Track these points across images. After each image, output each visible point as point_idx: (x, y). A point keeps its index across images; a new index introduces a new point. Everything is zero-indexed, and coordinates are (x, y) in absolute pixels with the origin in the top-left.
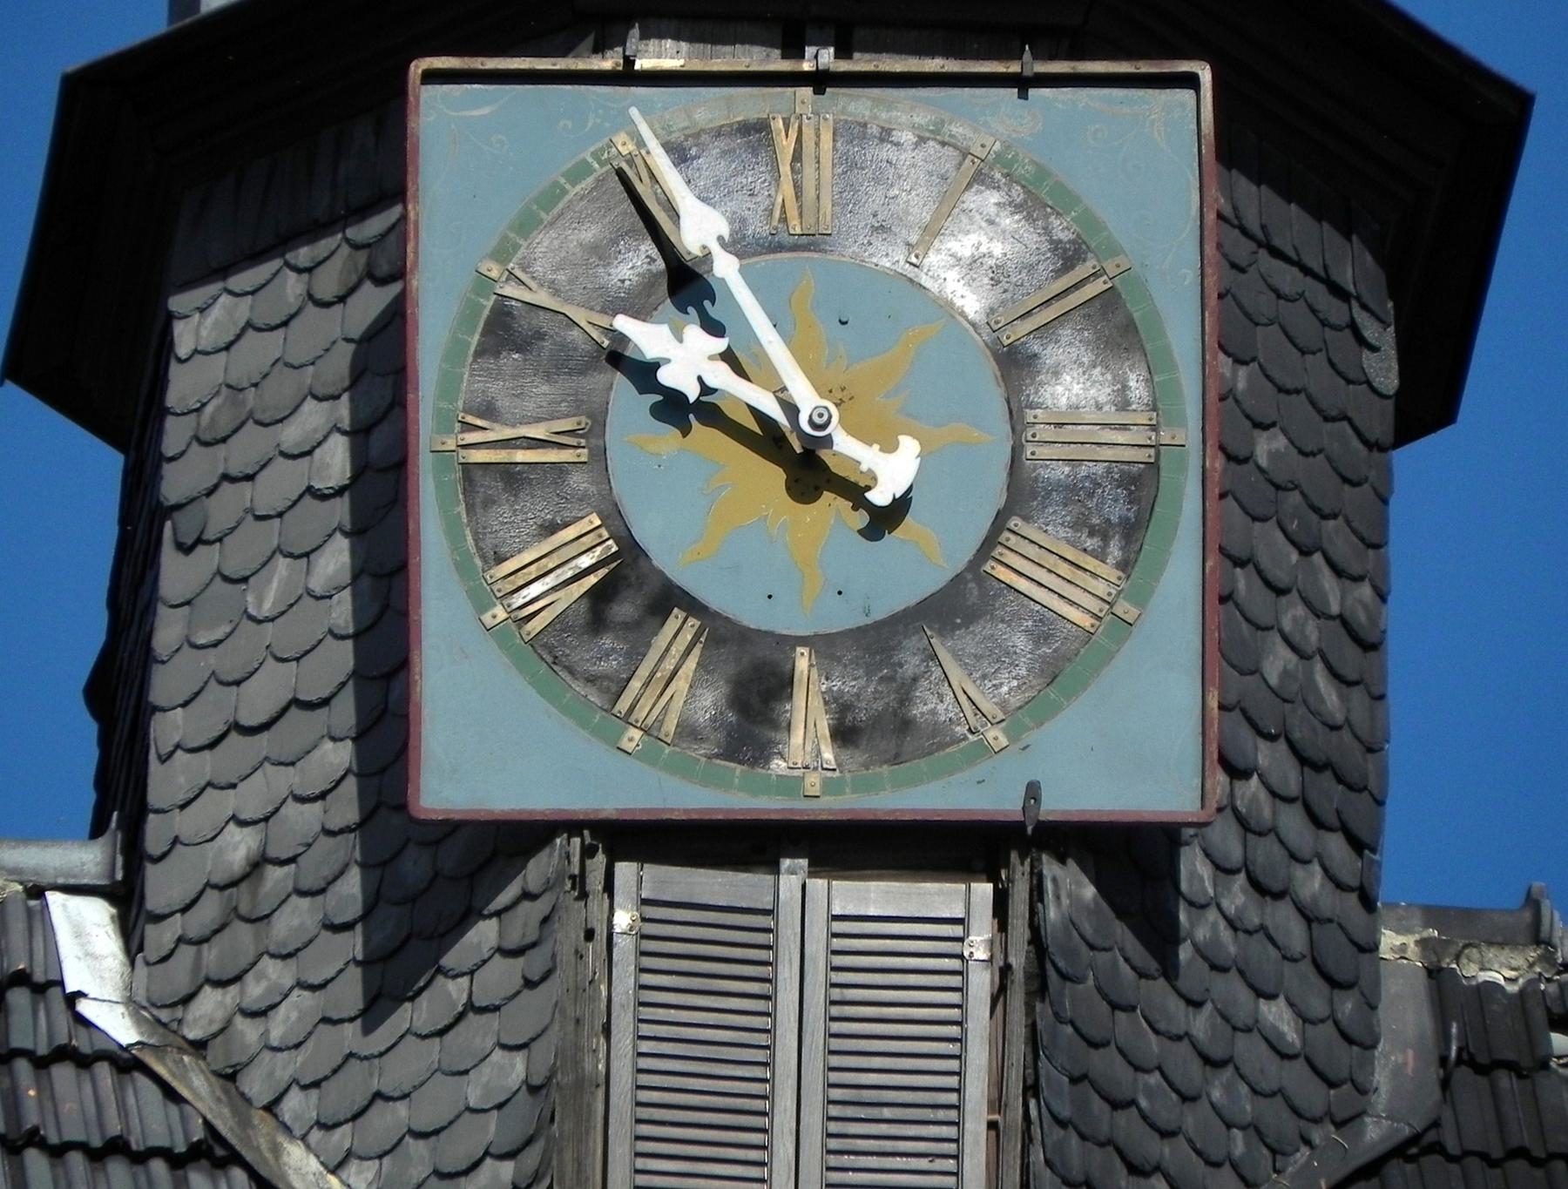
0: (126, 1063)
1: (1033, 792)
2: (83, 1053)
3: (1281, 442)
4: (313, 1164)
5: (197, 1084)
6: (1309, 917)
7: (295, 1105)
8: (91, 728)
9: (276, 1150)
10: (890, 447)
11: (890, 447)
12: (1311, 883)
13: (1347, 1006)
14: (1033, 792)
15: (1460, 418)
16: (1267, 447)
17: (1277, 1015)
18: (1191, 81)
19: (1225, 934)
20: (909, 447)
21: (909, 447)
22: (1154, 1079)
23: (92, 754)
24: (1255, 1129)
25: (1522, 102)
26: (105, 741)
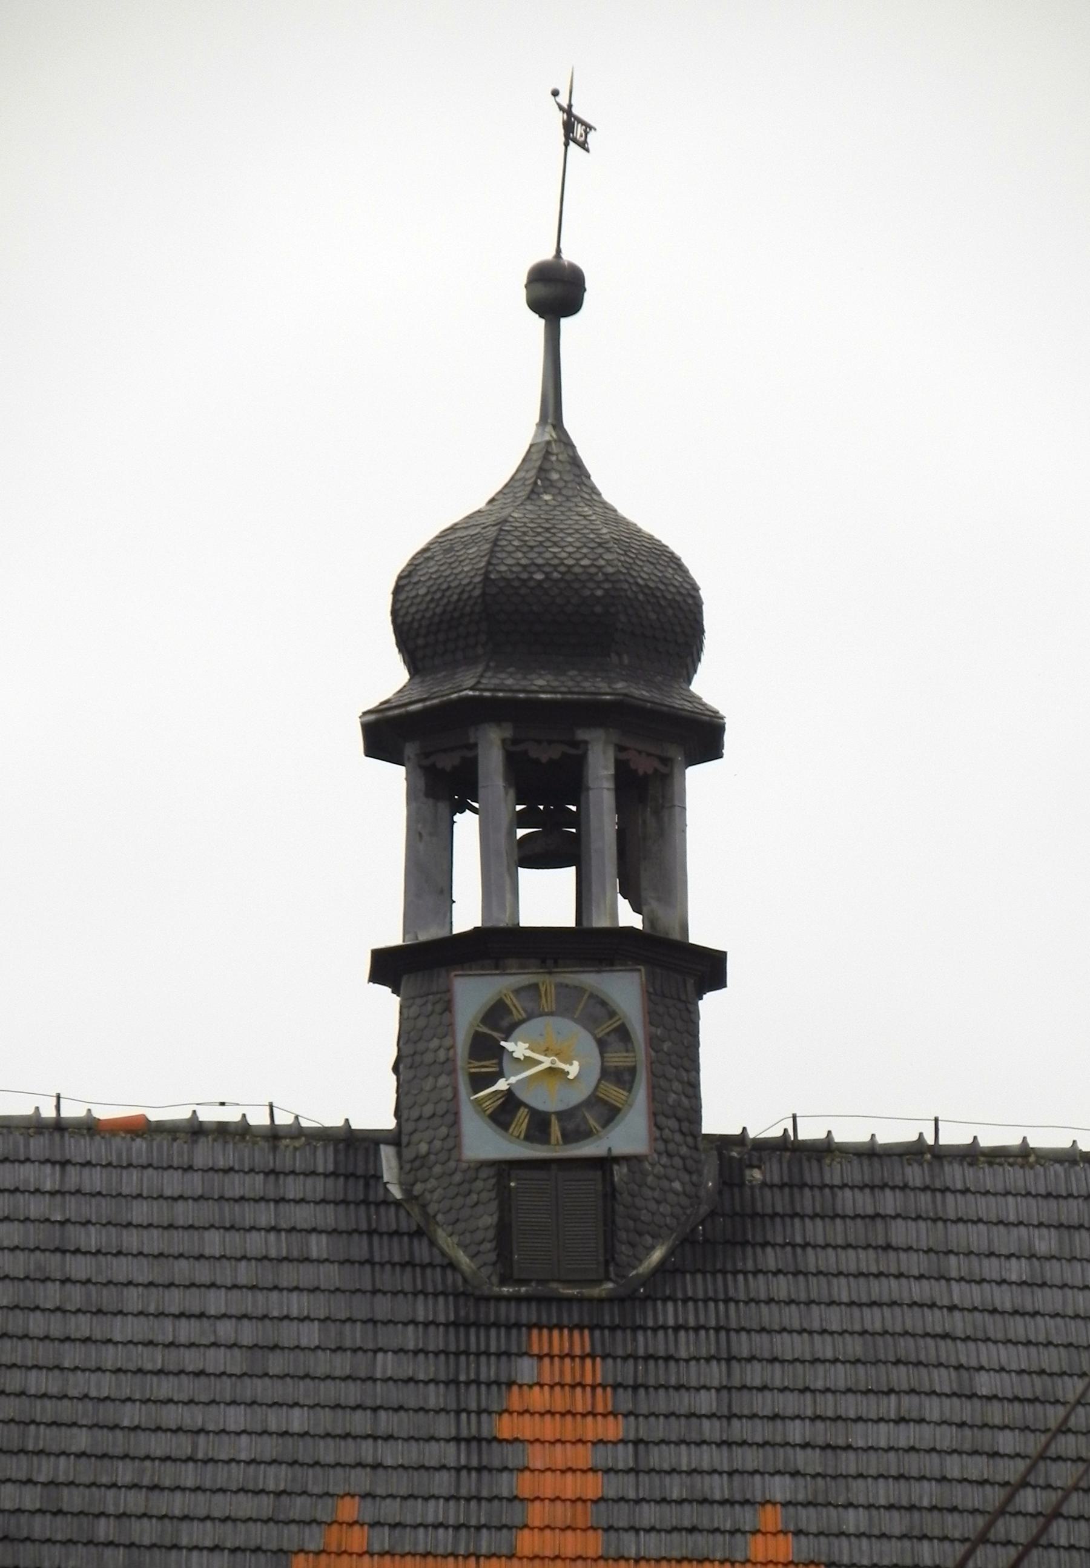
0: (397, 1204)
1: (610, 1149)
2: (388, 1202)
3: (670, 1044)
4: (444, 1235)
5: (416, 1211)
6: (683, 1158)
7: (440, 1217)
8: (395, 1077)
9: (435, 1231)
10: (571, 1064)
11: (571, 1064)
12: (684, 1150)
13: (695, 1178)
14: (610, 1149)
15: (725, 751)
16: (666, 1046)
17: (677, 1185)
18: (639, 970)
19: (662, 1169)
20: (576, 1063)
21: (576, 1063)
22: (644, 1211)
23: (395, 1084)
24: (672, 1215)
25: (725, 986)
26: (398, 1080)
